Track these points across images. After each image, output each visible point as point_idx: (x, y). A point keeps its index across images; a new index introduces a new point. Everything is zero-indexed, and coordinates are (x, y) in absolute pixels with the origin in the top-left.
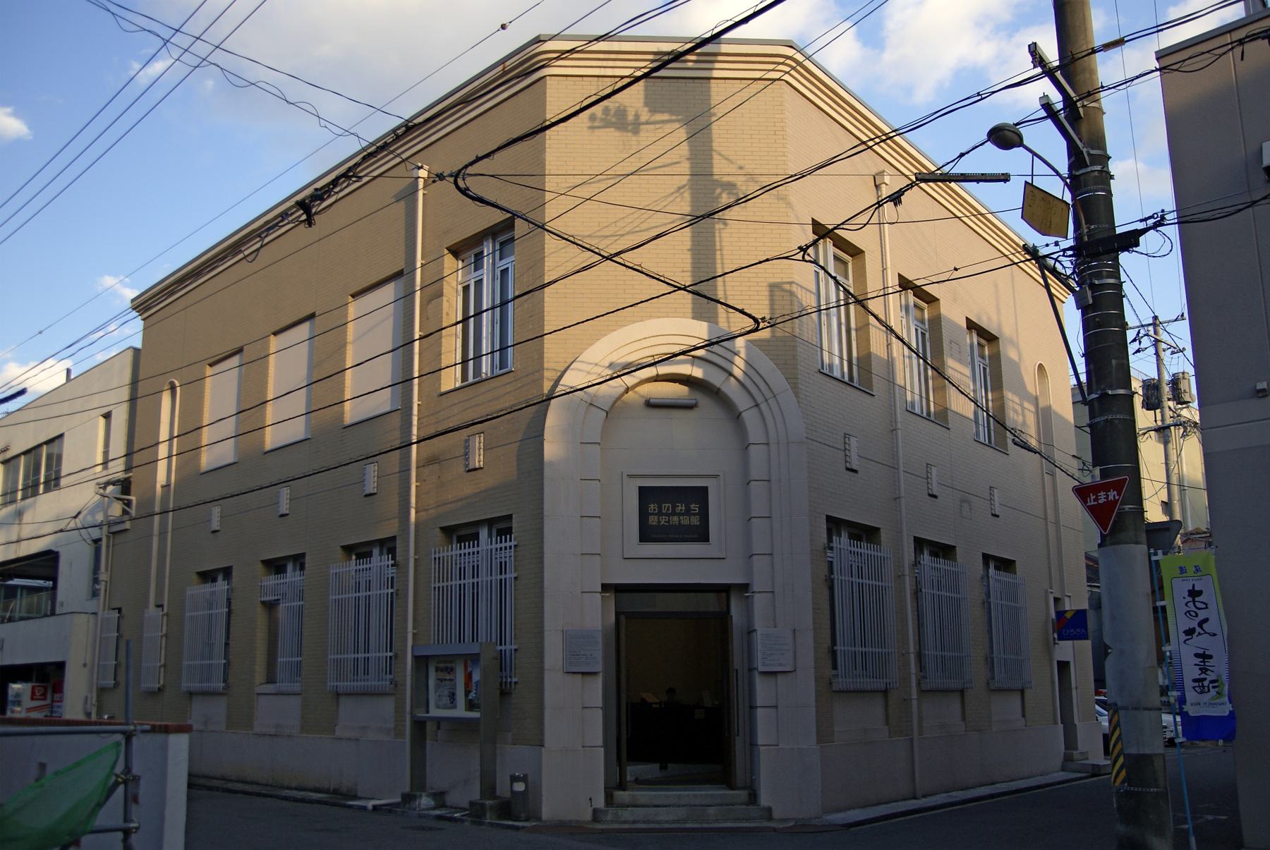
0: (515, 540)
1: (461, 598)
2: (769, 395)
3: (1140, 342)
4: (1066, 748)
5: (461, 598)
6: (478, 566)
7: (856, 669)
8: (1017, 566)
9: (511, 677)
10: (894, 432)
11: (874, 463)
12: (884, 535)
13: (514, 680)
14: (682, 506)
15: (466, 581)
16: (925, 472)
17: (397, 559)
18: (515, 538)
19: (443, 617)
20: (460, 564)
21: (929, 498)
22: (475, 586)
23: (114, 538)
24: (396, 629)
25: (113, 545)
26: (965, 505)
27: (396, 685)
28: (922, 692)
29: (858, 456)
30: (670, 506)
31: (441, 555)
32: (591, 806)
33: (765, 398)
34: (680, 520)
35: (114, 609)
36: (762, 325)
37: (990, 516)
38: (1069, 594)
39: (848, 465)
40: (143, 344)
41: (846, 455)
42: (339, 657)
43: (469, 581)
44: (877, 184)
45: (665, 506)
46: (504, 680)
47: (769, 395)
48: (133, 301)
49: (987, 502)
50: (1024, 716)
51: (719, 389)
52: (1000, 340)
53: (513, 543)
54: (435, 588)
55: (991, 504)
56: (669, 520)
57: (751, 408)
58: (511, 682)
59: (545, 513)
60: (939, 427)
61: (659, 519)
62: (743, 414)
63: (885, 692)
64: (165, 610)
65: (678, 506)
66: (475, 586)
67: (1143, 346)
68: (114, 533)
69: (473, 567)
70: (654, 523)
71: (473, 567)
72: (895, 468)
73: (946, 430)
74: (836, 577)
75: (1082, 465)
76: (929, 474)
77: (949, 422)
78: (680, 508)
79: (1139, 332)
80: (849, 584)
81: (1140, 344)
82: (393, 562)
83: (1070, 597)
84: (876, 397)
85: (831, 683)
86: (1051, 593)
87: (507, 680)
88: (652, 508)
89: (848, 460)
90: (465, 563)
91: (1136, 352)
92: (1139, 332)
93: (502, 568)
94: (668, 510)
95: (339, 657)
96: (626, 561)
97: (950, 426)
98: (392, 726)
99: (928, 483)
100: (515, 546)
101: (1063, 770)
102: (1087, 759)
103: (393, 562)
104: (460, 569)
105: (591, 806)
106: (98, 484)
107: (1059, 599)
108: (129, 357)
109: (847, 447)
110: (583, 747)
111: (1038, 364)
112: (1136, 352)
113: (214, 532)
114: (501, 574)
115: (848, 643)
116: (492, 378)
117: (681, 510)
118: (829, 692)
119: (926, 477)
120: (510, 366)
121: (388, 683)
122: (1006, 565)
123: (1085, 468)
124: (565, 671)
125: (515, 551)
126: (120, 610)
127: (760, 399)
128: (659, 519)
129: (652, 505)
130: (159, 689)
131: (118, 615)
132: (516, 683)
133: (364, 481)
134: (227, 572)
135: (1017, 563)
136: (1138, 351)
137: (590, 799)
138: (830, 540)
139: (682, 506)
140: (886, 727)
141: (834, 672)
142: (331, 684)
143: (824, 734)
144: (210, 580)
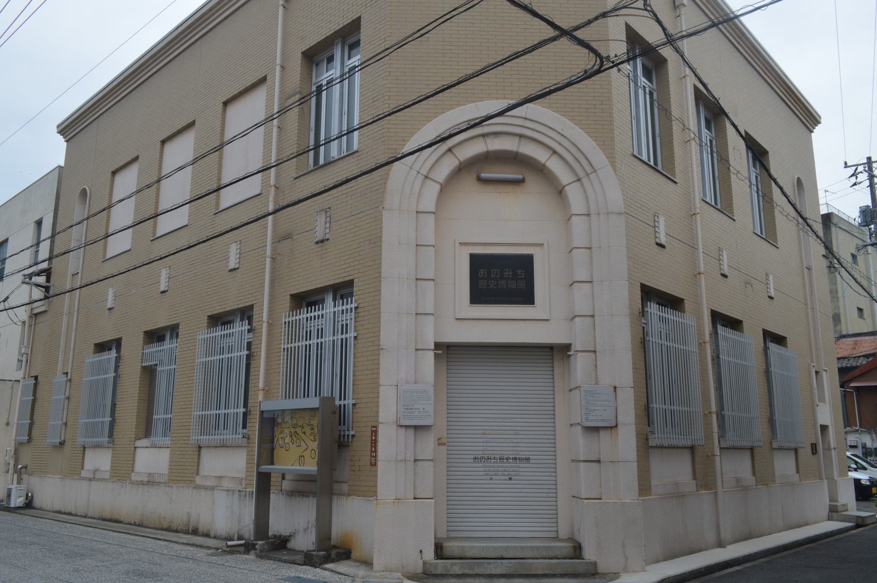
0: (356, 302)
1: (308, 358)
2: (589, 170)
3: (857, 178)
4: (830, 501)
5: (308, 358)
6: (322, 329)
7: (666, 427)
8: (788, 342)
9: (348, 430)
10: (694, 217)
11: (678, 242)
12: (687, 305)
13: (352, 433)
14: (509, 272)
15: (311, 342)
16: (718, 254)
17: (254, 324)
18: (356, 300)
19: (290, 376)
20: (307, 327)
21: (721, 277)
22: (320, 346)
23: (35, 319)
24: (502, 563)
25: (35, 324)
26: (748, 286)
27: (248, 439)
28: (721, 449)
29: (666, 234)
30: (499, 271)
31: (290, 320)
32: (422, 558)
33: (587, 173)
34: (507, 284)
35: (32, 377)
36: (607, 65)
37: (767, 298)
38: (826, 369)
39: (658, 240)
40: (65, 165)
41: (656, 232)
42: (203, 413)
43: (314, 341)
44: (676, 5)
45: (494, 271)
46: (342, 433)
47: (589, 170)
48: (58, 126)
49: (764, 285)
50: (798, 472)
51: (544, 165)
52: (769, 153)
53: (353, 306)
54: (284, 349)
55: (768, 288)
56: (498, 284)
57: (573, 182)
58: (348, 435)
59: (383, 275)
60: (727, 218)
61: (488, 283)
62: (567, 188)
63: (692, 448)
64: (69, 377)
65: (506, 271)
66: (320, 346)
67: (859, 180)
68: (36, 315)
69: (318, 330)
70: (484, 287)
71: (318, 330)
72: (694, 247)
73: (732, 221)
74: (651, 339)
75: (830, 263)
76: (721, 257)
77: (735, 214)
78: (507, 273)
79: (856, 169)
80: (665, 347)
81: (856, 178)
82: (249, 327)
83: (826, 371)
84: (678, 184)
85: (647, 439)
86: (814, 366)
87: (345, 433)
88: (482, 273)
89: (657, 235)
90: (311, 327)
91: (853, 185)
92: (856, 169)
93: (345, 329)
94: (497, 274)
95: (203, 413)
96: (459, 322)
97: (735, 218)
98: (244, 476)
99: (720, 264)
100: (356, 308)
101: (830, 519)
102: (847, 510)
103: (249, 327)
104: (307, 332)
105: (422, 558)
106: (24, 275)
107: (819, 372)
108: (56, 173)
109: (657, 224)
110: (415, 499)
111: (796, 178)
112: (853, 185)
113: (109, 309)
114: (346, 339)
115: (659, 402)
116: (339, 159)
117: (509, 275)
118: (645, 447)
119: (718, 259)
120: (355, 148)
121: (241, 436)
122: (780, 340)
123: (832, 266)
124: (398, 424)
125: (355, 313)
126: (36, 378)
127: (581, 174)
128: (488, 283)
129: (482, 270)
130: (60, 443)
131: (34, 382)
132: (353, 436)
133: (229, 258)
134: (118, 342)
135: (788, 339)
136: (855, 184)
137: (421, 551)
138: (643, 305)
139: (509, 272)
140: (694, 481)
141: (649, 429)
142: (194, 438)
143: (644, 487)
144: (107, 350)
